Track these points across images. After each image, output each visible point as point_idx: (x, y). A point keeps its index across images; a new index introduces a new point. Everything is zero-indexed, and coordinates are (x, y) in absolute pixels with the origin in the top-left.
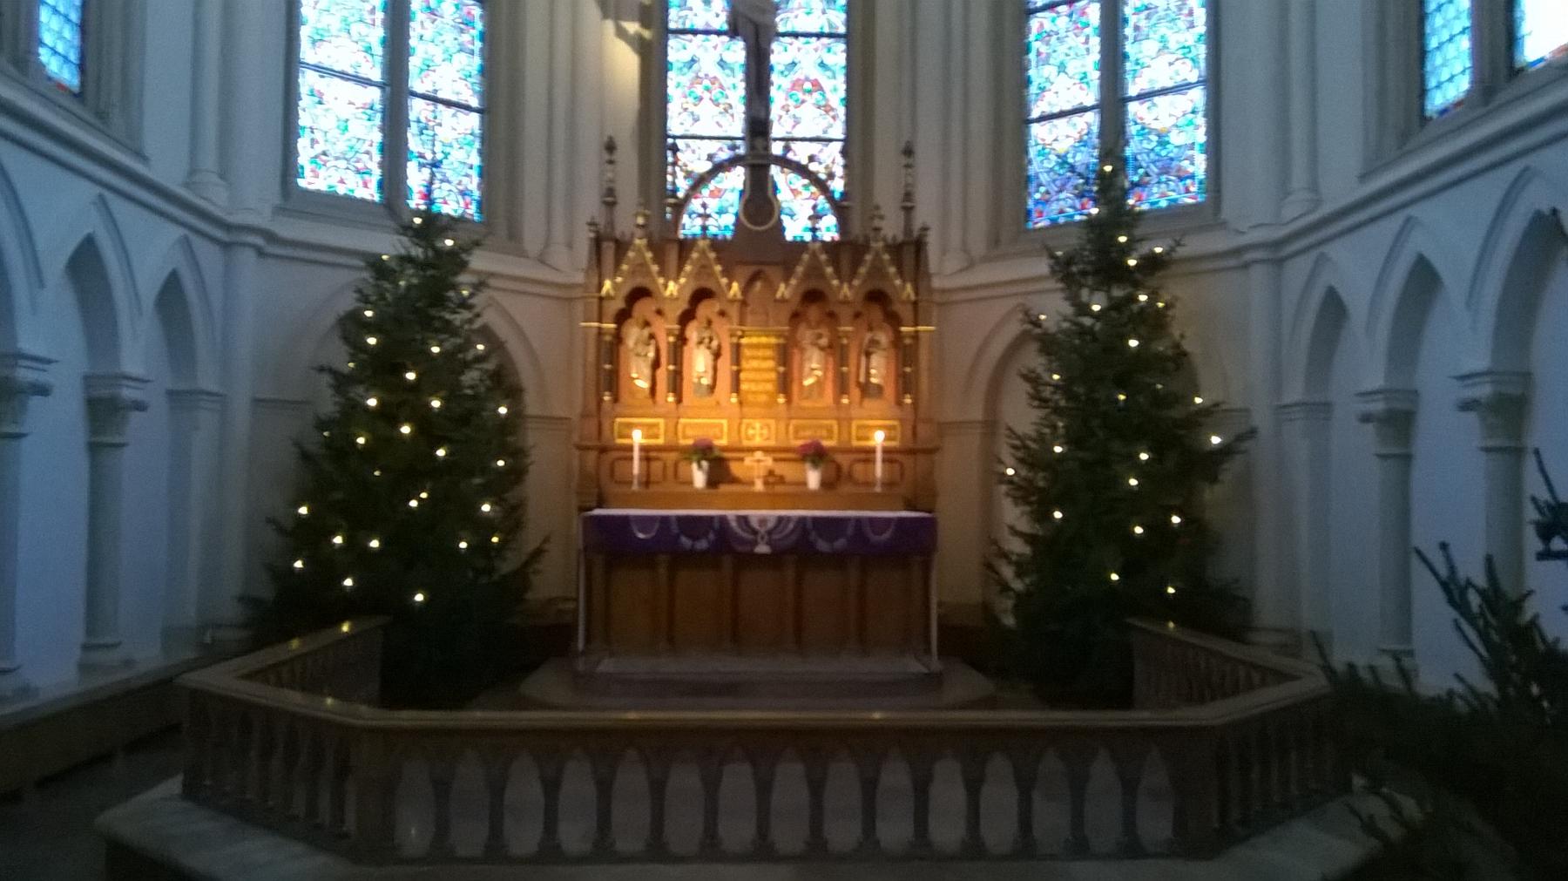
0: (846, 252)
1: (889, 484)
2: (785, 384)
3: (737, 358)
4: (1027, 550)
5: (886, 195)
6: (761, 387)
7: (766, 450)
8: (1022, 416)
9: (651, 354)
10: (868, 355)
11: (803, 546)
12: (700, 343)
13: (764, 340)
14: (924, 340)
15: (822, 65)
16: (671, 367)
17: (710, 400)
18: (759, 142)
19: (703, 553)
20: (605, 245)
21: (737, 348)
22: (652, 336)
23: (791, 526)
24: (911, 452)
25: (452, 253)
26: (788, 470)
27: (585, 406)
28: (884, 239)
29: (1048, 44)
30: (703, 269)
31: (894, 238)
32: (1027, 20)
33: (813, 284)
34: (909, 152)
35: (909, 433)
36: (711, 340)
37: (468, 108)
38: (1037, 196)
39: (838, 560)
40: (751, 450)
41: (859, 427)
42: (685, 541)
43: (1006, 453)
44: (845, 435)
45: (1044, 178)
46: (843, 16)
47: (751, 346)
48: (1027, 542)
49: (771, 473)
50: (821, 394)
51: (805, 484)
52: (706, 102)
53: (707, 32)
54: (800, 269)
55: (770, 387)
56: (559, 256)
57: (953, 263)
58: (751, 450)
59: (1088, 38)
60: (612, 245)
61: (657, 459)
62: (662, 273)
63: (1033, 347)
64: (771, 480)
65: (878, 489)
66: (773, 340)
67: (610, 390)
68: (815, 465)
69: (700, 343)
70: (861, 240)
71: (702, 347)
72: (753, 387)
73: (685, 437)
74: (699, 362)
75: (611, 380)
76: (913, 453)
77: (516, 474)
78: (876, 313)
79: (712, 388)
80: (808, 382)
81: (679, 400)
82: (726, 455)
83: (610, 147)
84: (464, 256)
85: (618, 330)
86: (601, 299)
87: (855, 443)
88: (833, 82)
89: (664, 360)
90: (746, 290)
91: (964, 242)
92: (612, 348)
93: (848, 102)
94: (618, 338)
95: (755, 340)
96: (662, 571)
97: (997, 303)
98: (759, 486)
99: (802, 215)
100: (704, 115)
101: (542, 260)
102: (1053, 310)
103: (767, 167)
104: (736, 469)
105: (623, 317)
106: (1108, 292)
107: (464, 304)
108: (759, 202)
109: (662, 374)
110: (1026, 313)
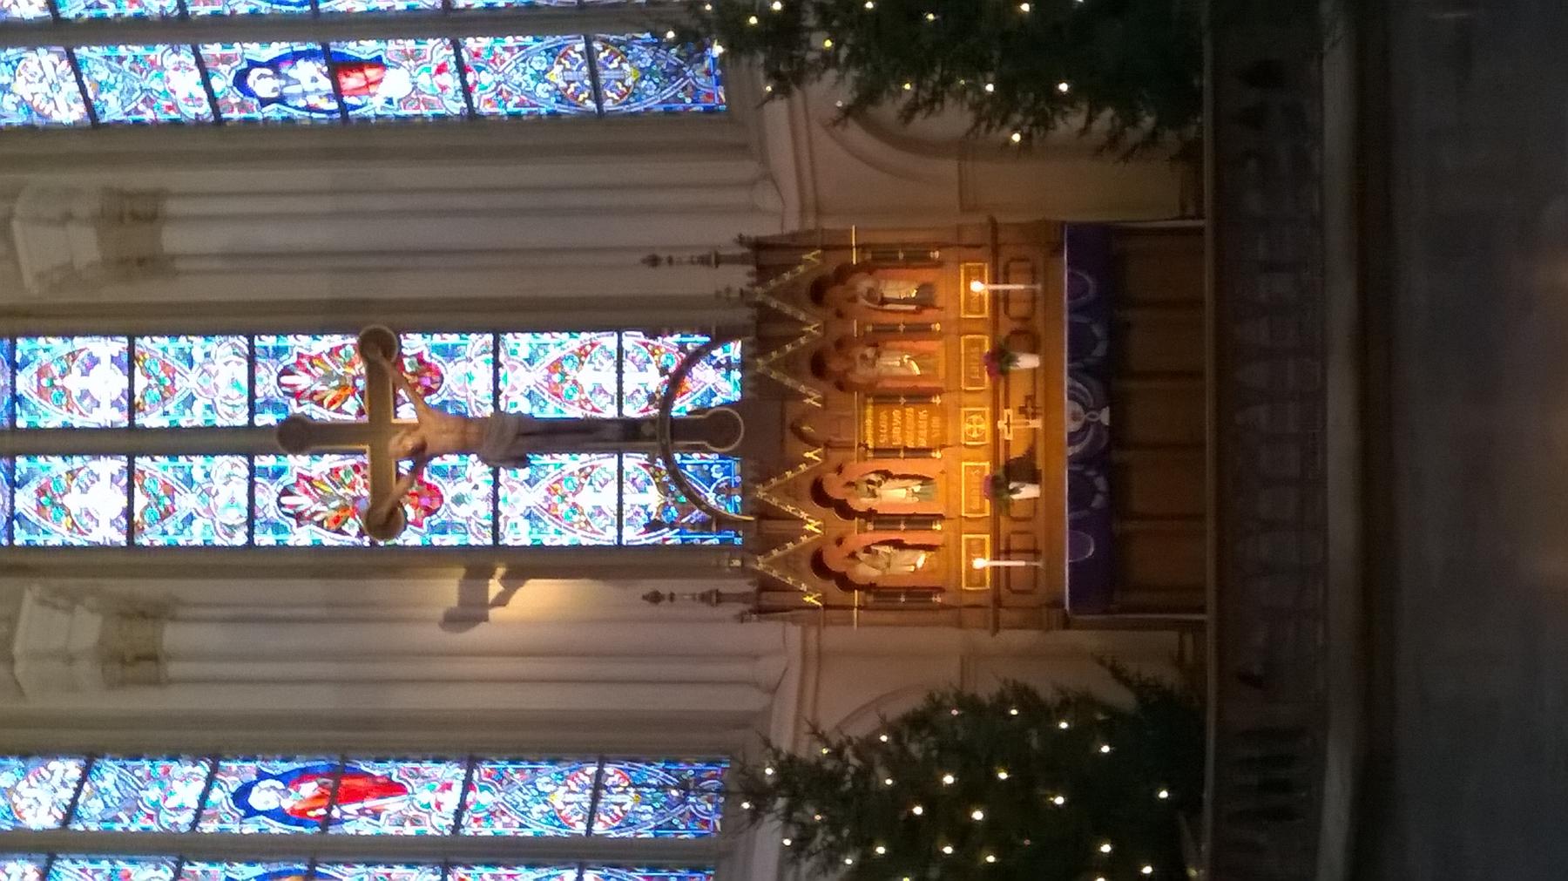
0: (763, 331)
1: (1033, 275)
2: (919, 397)
3: (891, 452)
4: (1108, 113)
5: (705, 282)
6: (923, 425)
7: (996, 417)
8: (953, 119)
9: (887, 549)
10: (884, 301)
11: (1102, 368)
12: (874, 495)
13: (869, 422)
14: (865, 240)
15: (530, 361)
16: (902, 527)
17: (940, 483)
18: (647, 430)
19: (1111, 486)
20: (765, 603)
21: (880, 452)
22: (867, 550)
23: (1079, 385)
24: (996, 251)
25: (779, 769)
26: (1017, 399)
27: (950, 624)
28: (752, 285)
29: (510, 93)
30: (790, 492)
31: (750, 274)
32: (482, 116)
33: (805, 365)
34: (654, 261)
35: (974, 252)
36: (870, 482)
37: (599, 774)
38: (688, 100)
39: (1117, 333)
40: (996, 433)
41: (968, 309)
42: (1098, 502)
43: (996, 136)
44: (979, 327)
45: (668, 93)
46: (473, 336)
47: (876, 436)
48: (1100, 110)
49: (1022, 410)
50: (930, 354)
51: (1034, 370)
52: (578, 499)
53: (495, 499)
54: (789, 382)
55: (923, 414)
56: (769, 669)
57: (767, 199)
58: (996, 433)
59: (505, 49)
60: (764, 595)
61: (1008, 541)
62: (795, 540)
63: (871, 110)
64: (1030, 410)
65: (1039, 287)
66: (869, 411)
67: (930, 595)
68: (1012, 360)
69: (874, 495)
70: (755, 311)
71: (878, 491)
72: (924, 433)
73: (981, 511)
74: (895, 496)
75: (917, 597)
76: (997, 252)
77: (1024, 695)
78: (837, 292)
79: (925, 480)
80: (916, 370)
81: (940, 517)
82: (1002, 462)
83: (655, 598)
84: (782, 757)
85: (860, 588)
86: (826, 607)
87: (986, 314)
88: (550, 348)
89: (894, 536)
90: (812, 443)
91: (741, 185)
92: (882, 595)
93: (574, 328)
94: (870, 588)
95: (869, 432)
96: (1131, 526)
97: (815, 153)
98: (1037, 424)
99: (716, 383)
100: (606, 500)
101: (773, 690)
102: (831, 92)
103: (674, 421)
104: (1017, 452)
105: (845, 583)
106: (811, 30)
107: (837, 753)
108: (710, 428)
109: (909, 539)
110: (835, 123)
